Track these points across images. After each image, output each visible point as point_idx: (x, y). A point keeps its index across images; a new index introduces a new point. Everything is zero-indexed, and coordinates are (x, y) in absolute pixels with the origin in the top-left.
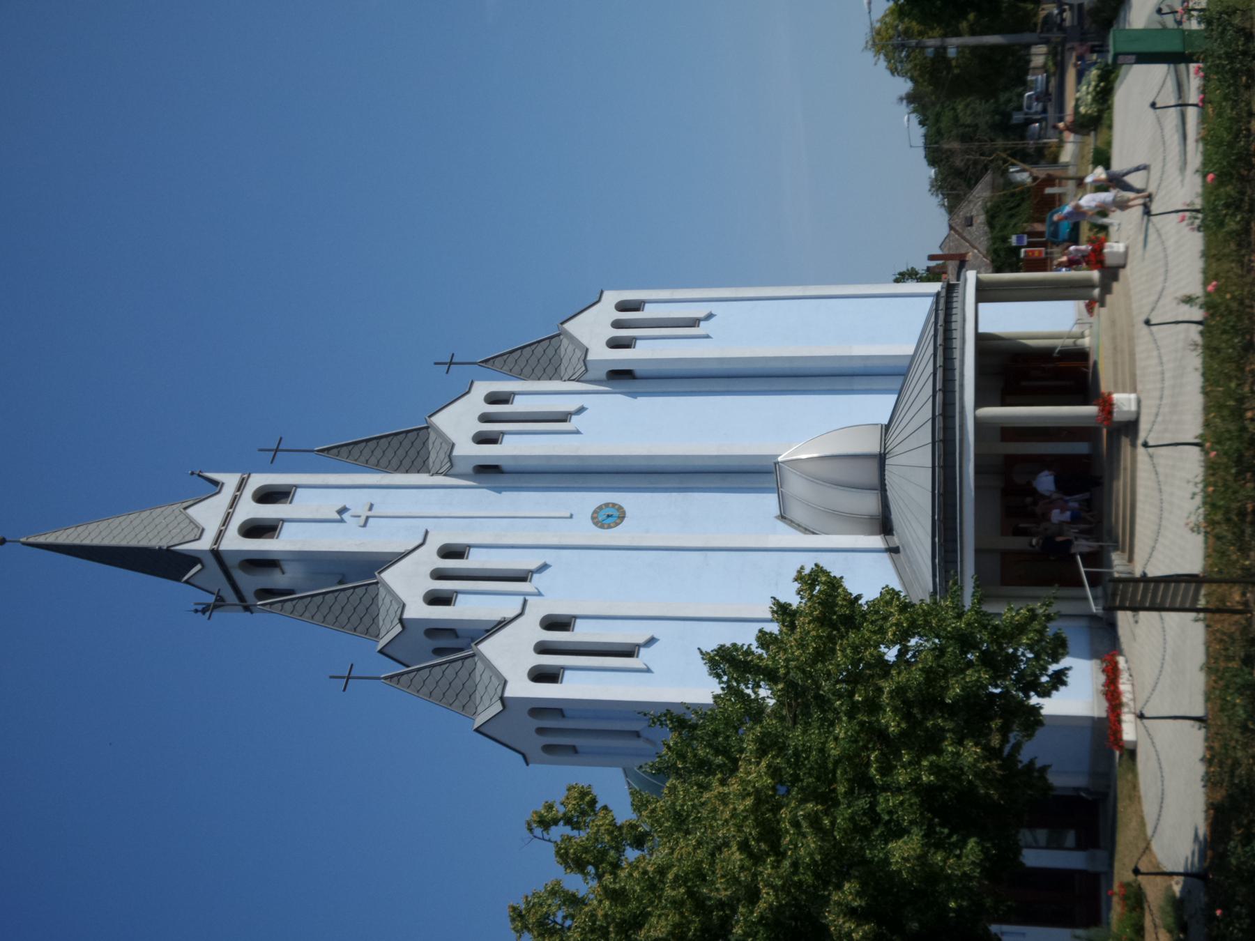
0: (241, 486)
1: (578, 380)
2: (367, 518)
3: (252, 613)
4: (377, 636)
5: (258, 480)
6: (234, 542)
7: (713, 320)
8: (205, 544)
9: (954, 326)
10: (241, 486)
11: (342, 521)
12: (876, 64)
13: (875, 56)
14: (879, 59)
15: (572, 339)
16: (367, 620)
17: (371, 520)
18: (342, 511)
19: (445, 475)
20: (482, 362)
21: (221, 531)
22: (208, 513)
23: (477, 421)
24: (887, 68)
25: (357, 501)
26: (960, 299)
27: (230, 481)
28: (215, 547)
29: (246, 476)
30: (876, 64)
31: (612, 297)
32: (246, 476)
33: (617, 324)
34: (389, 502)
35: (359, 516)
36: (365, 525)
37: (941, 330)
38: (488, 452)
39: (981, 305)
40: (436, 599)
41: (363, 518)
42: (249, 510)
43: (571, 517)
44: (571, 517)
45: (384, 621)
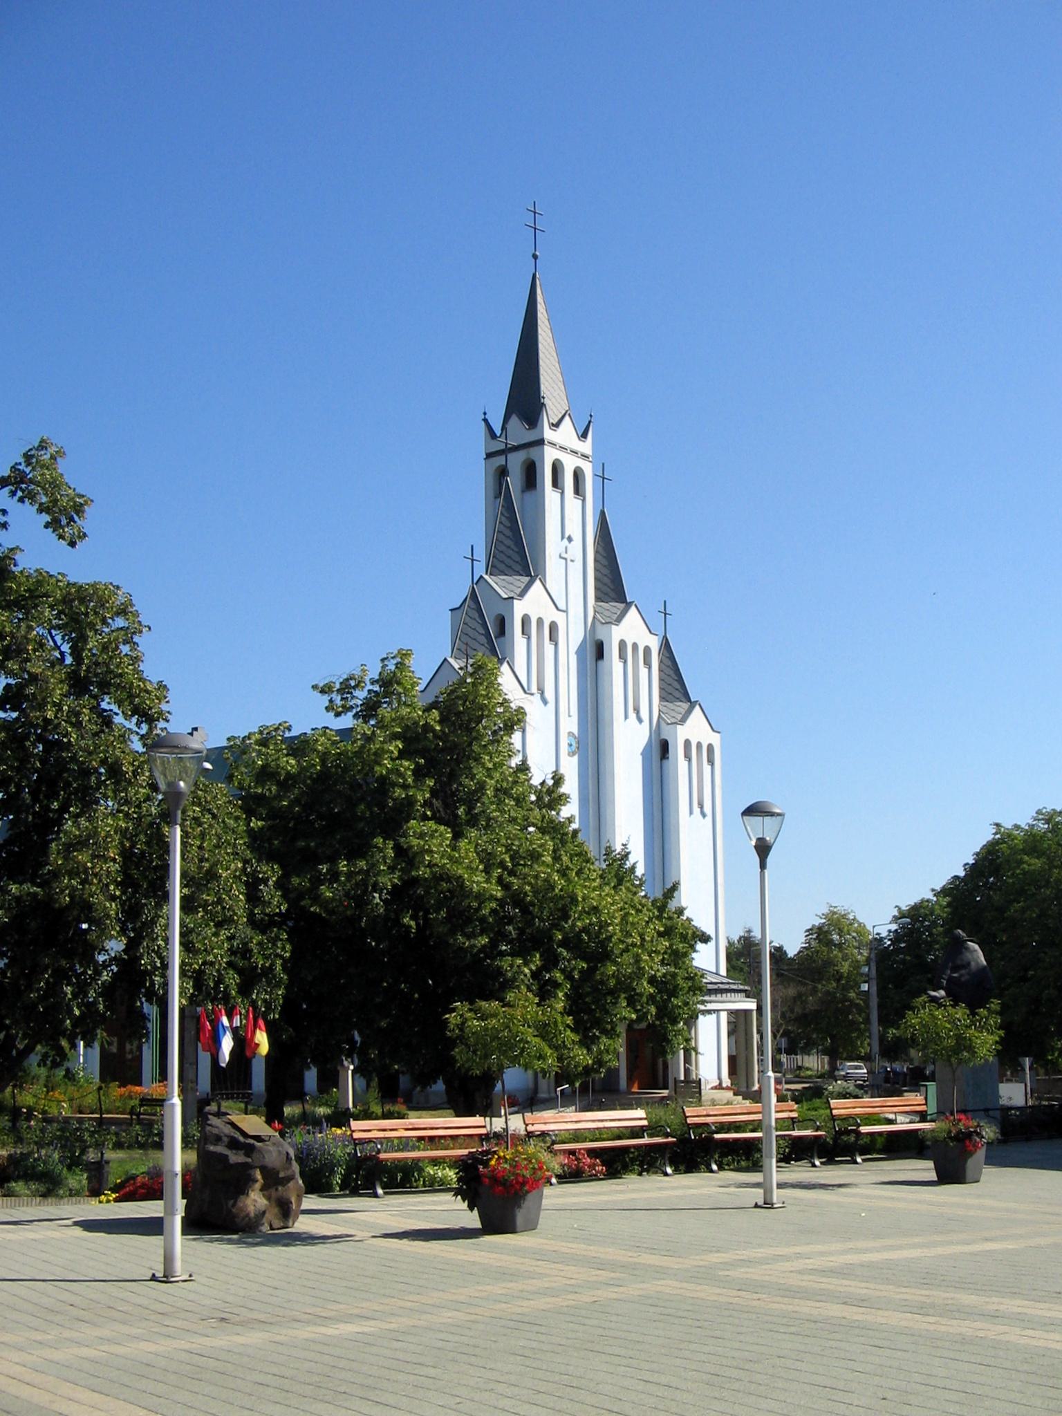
0: (585, 456)
1: (659, 716)
2: (566, 559)
3: (485, 459)
4: (491, 574)
5: (587, 468)
6: (550, 455)
7: (701, 817)
8: (548, 434)
9: (719, 995)
10: (585, 456)
11: (563, 538)
12: (817, 915)
13: (823, 914)
14: (821, 918)
15: (689, 712)
16: (502, 567)
17: (564, 561)
18: (570, 539)
19: (594, 617)
20: (667, 639)
21: (555, 445)
22: (565, 435)
23: (633, 641)
24: (814, 926)
25: (575, 549)
26: (739, 999)
27: (586, 447)
28: (546, 442)
29: (591, 459)
30: (817, 915)
31: (715, 739)
32: (591, 459)
33: (699, 745)
34: (576, 570)
35: (566, 552)
36: (561, 557)
37: (716, 987)
38: (613, 651)
39: (726, 1012)
40: (526, 620)
41: (564, 555)
42: (570, 464)
43: (570, 716)
44: (570, 716)
45: (504, 580)
